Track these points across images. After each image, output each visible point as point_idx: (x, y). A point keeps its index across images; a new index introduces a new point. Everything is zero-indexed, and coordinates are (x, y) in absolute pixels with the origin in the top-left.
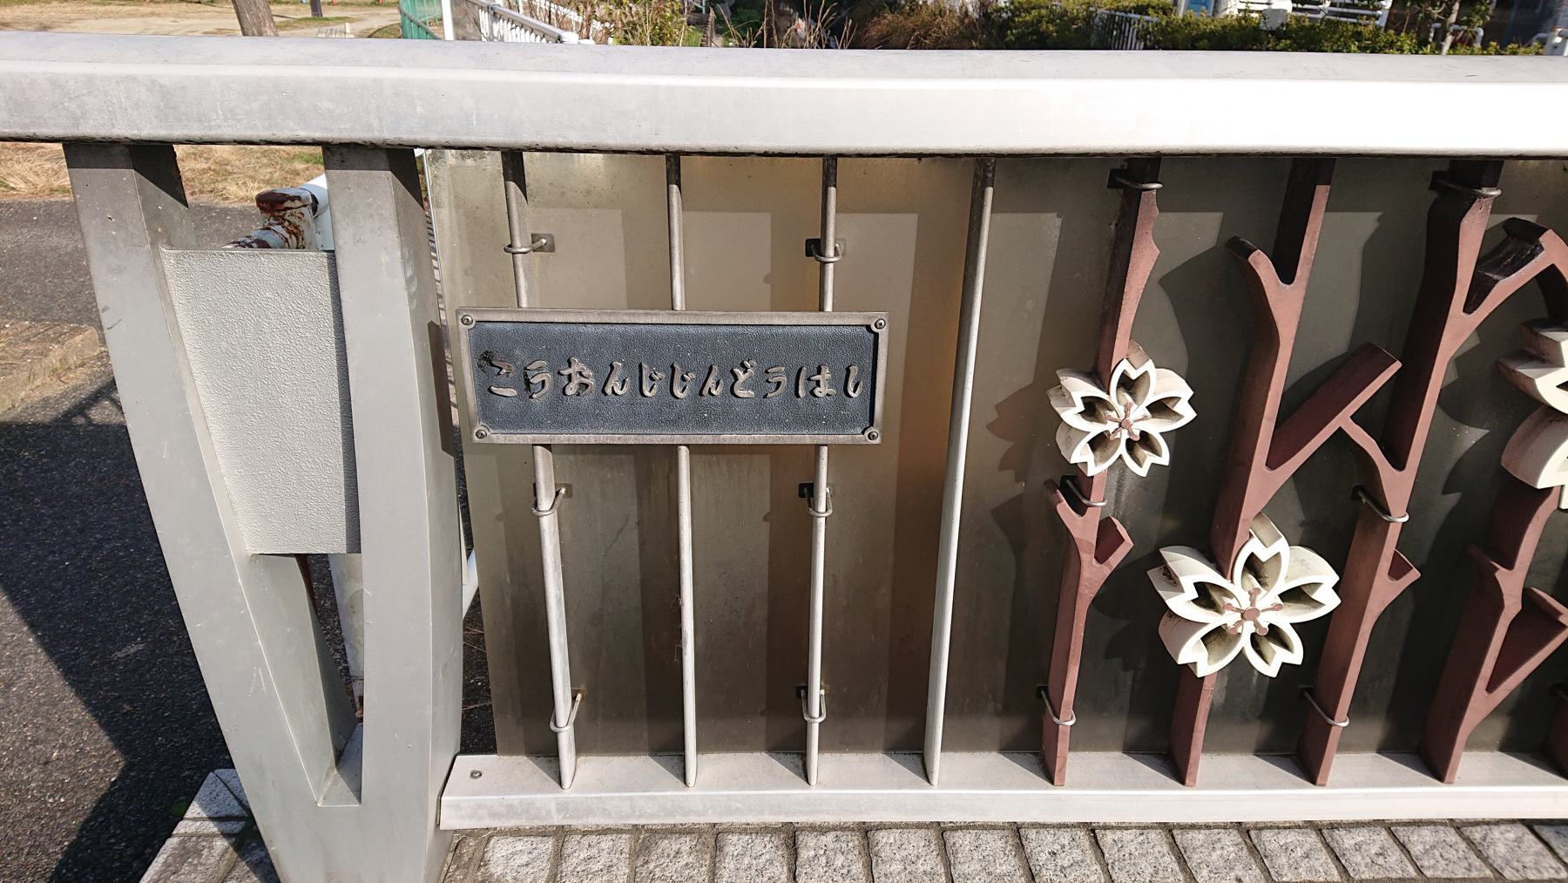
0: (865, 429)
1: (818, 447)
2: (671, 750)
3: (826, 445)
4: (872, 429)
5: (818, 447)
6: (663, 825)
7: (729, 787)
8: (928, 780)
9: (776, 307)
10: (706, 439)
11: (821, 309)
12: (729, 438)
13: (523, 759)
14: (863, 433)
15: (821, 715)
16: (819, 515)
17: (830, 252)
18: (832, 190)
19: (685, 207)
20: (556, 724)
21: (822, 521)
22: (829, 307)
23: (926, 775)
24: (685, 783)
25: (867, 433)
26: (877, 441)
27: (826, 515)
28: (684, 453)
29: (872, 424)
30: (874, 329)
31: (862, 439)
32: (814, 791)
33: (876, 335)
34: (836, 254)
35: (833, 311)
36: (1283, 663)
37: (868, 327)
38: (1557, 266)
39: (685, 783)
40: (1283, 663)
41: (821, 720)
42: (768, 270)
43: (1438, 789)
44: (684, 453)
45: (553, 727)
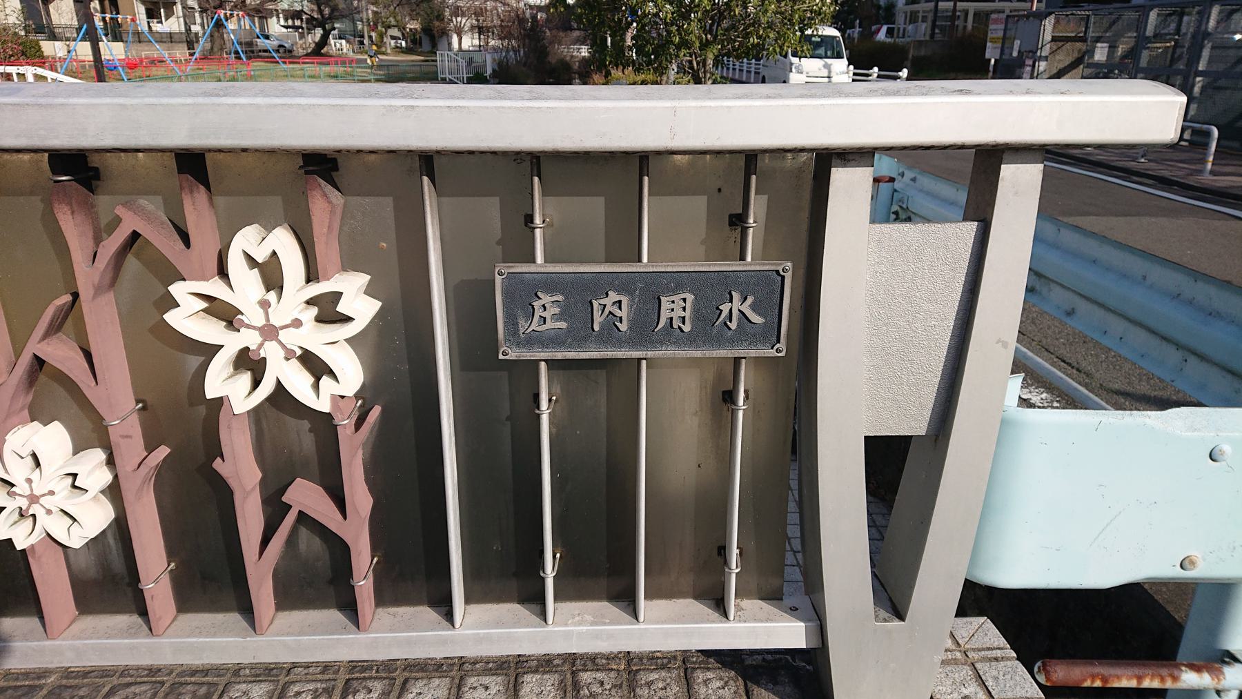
0: (774, 346)
1: (737, 361)
2: (534, 598)
3: (645, 359)
4: (778, 345)
5: (639, 360)
6: (39, 668)
7: (477, 628)
8: (637, 619)
9: (609, 260)
10: (559, 355)
11: (640, 260)
12: (572, 355)
13: (605, 604)
14: (772, 348)
15: (737, 567)
16: (739, 408)
17: (751, 221)
18: (646, 178)
19: (544, 193)
20: (544, 572)
21: (741, 414)
22: (749, 258)
23: (635, 615)
24: (546, 622)
25: (775, 348)
26: (501, 357)
27: (549, 411)
28: (543, 365)
29: (778, 341)
30: (782, 273)
31: (772, 353)
32: (456, 632)
33: (783, 278)
34: (755, 222)
35: (648, 262)
36: (11, 539)
37: (777, 272)
38: (727, 223)
39: (546, 622)
40: (11, 539)
41: (737, 571)
42: (704, 236)
43: (144, 641)
44: (543, 365)
45: (542, 574)
